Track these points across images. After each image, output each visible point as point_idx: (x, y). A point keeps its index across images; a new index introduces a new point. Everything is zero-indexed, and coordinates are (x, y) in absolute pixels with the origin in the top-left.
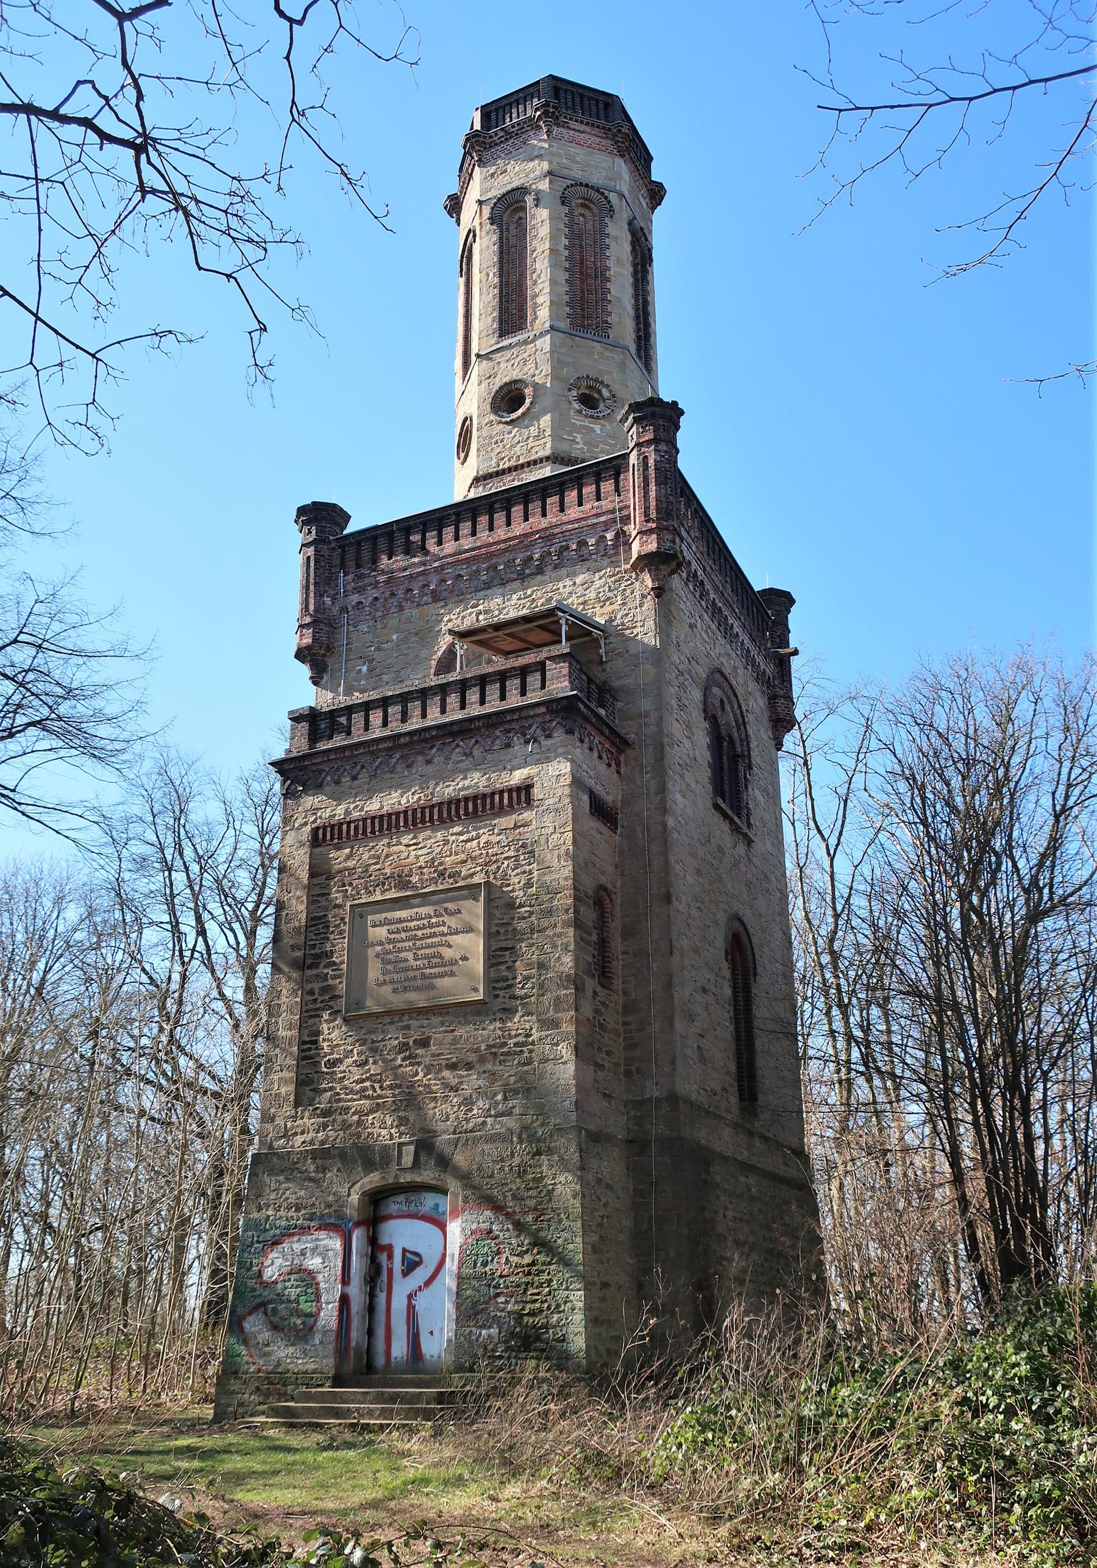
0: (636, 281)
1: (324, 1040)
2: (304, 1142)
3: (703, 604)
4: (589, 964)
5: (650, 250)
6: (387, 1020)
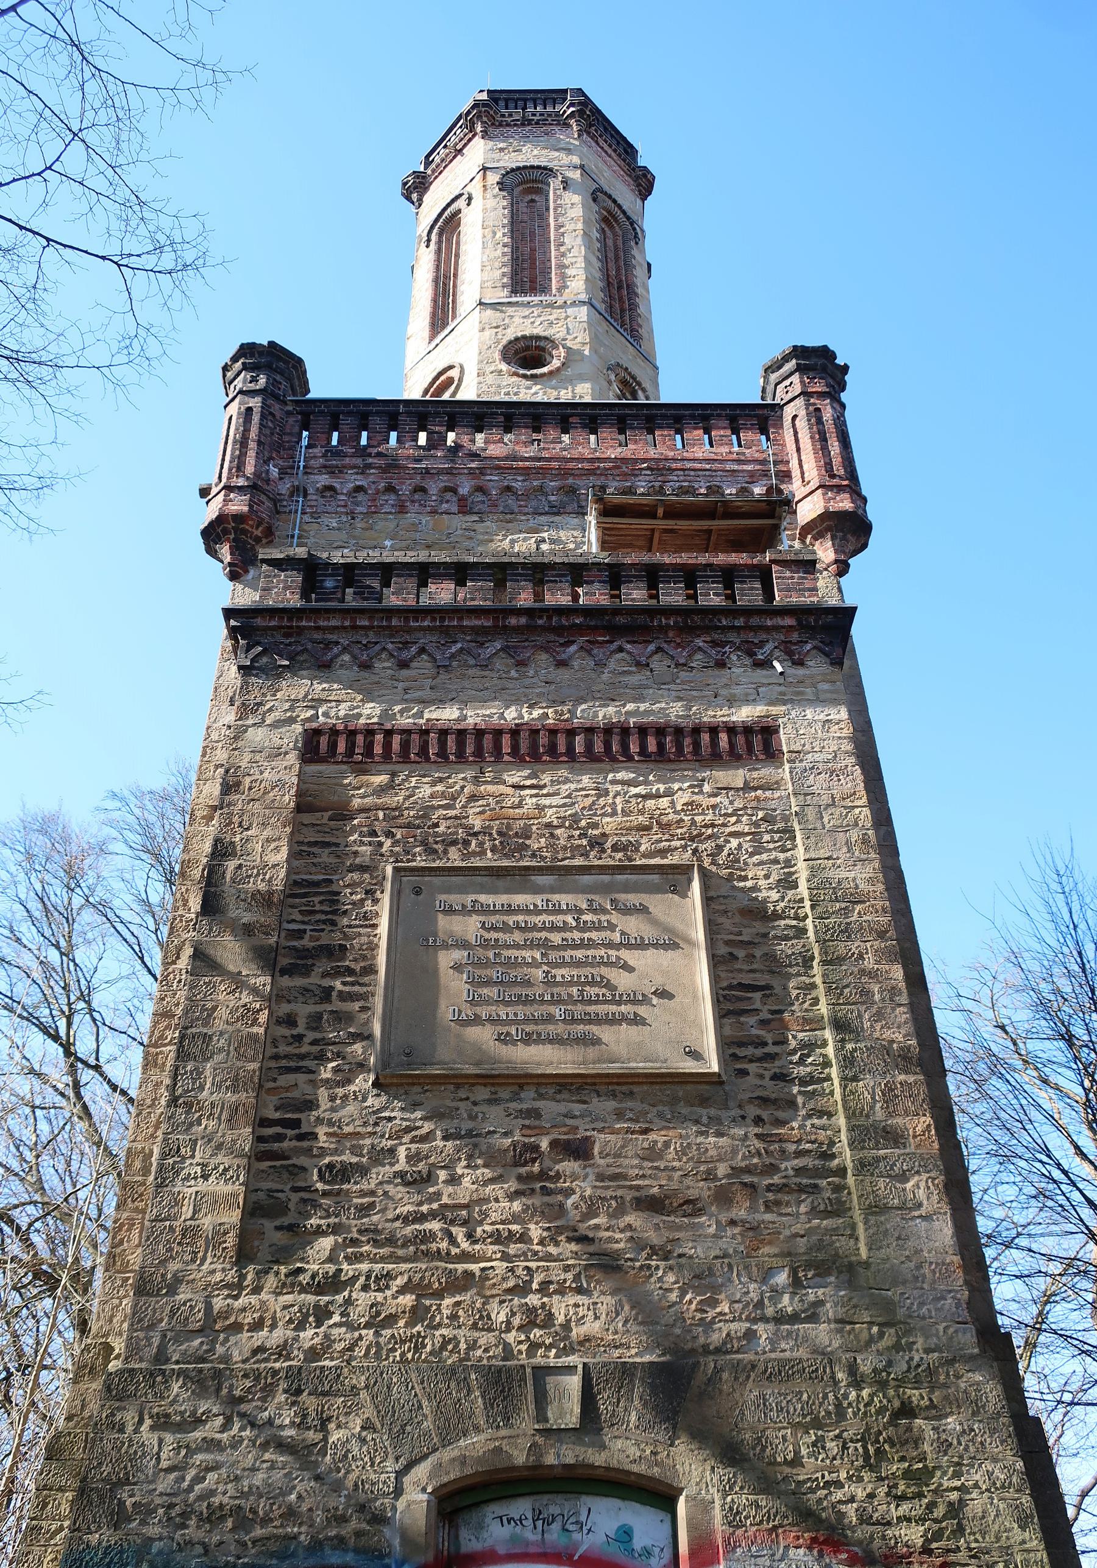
1: (319, 1121)
2: (256, 1351)
6: (482, 1093)
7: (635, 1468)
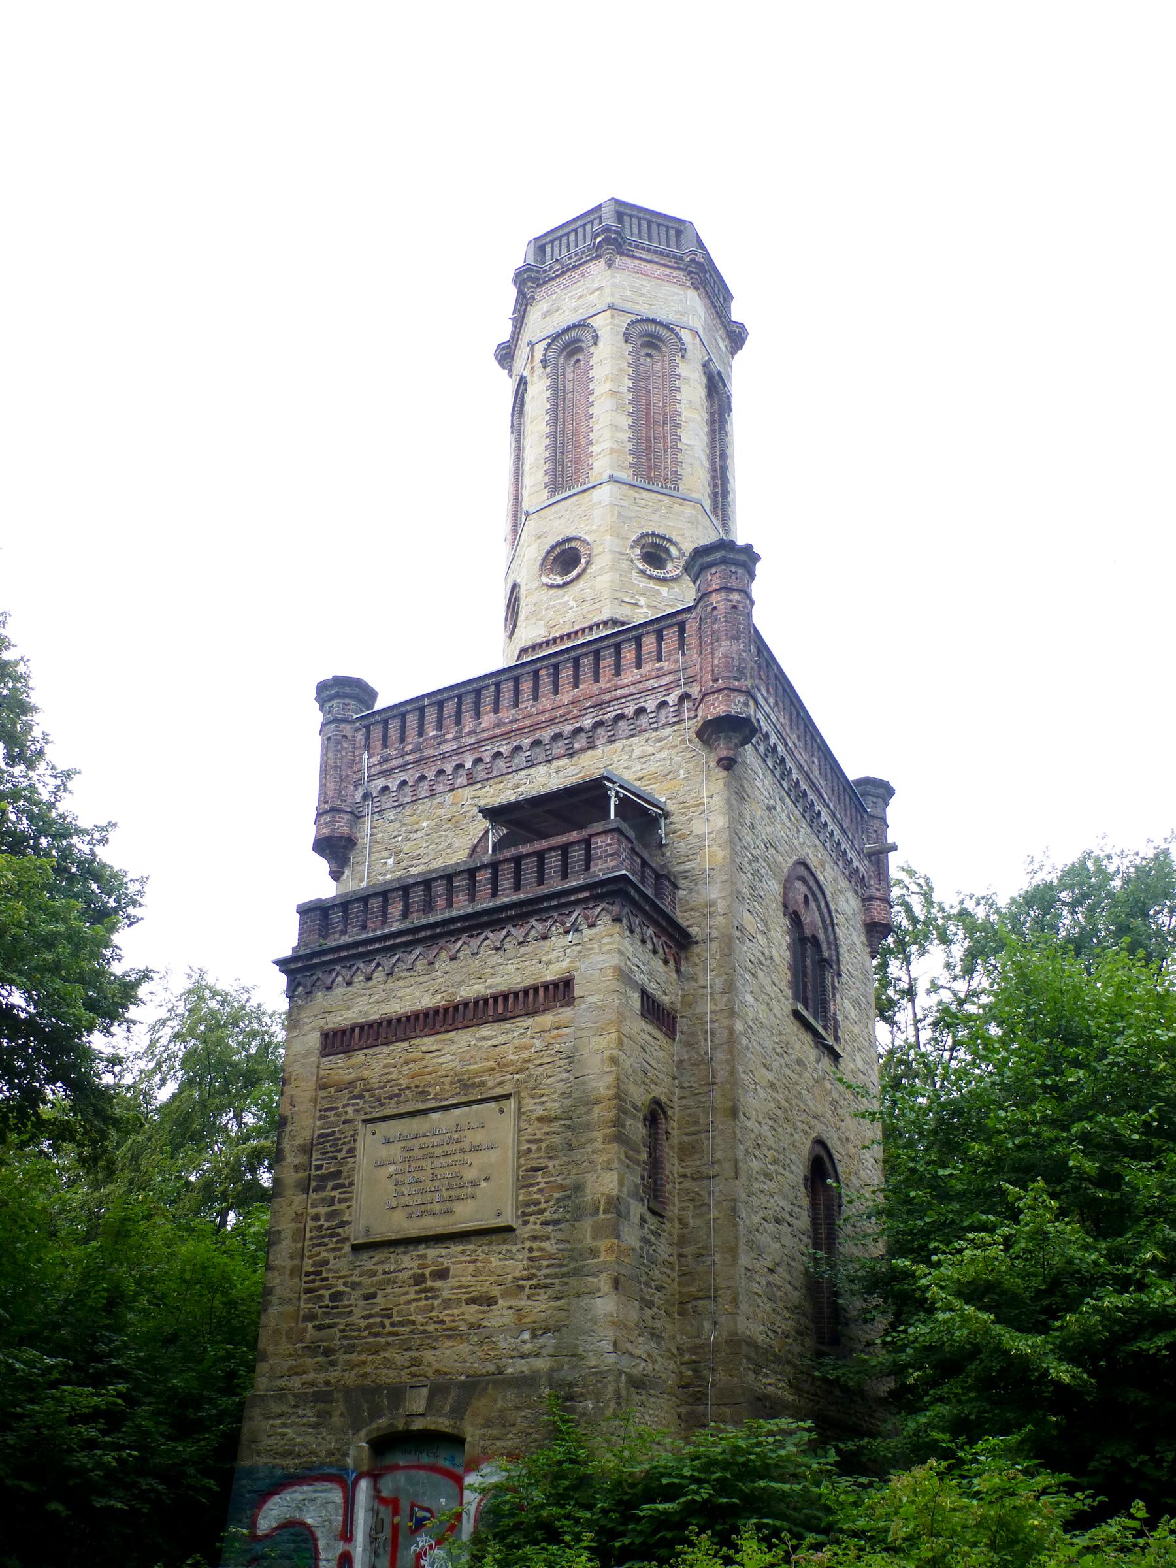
0: (712, 432)
2: (303, 1384)
3: (785, 784)
4: (636, 1186)
5: (729, 397)
7: (447, 1430)
